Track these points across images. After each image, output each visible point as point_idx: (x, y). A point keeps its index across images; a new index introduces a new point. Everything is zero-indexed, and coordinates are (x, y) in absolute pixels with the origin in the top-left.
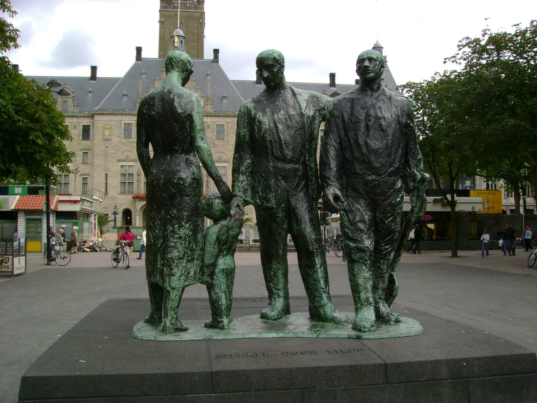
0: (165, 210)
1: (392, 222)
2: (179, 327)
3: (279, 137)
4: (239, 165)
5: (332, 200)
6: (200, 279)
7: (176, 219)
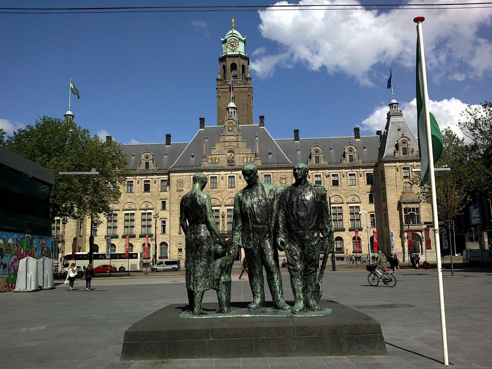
2: (201, 312)
3: (254, 211)
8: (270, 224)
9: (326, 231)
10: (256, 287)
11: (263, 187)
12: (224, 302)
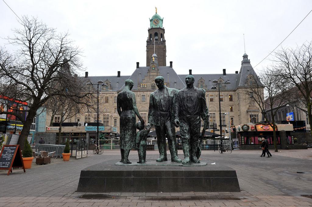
3: (161, 104)
5: (176, 124)
9: (205, 116)
11: (167, 90)
12: (142, 156)
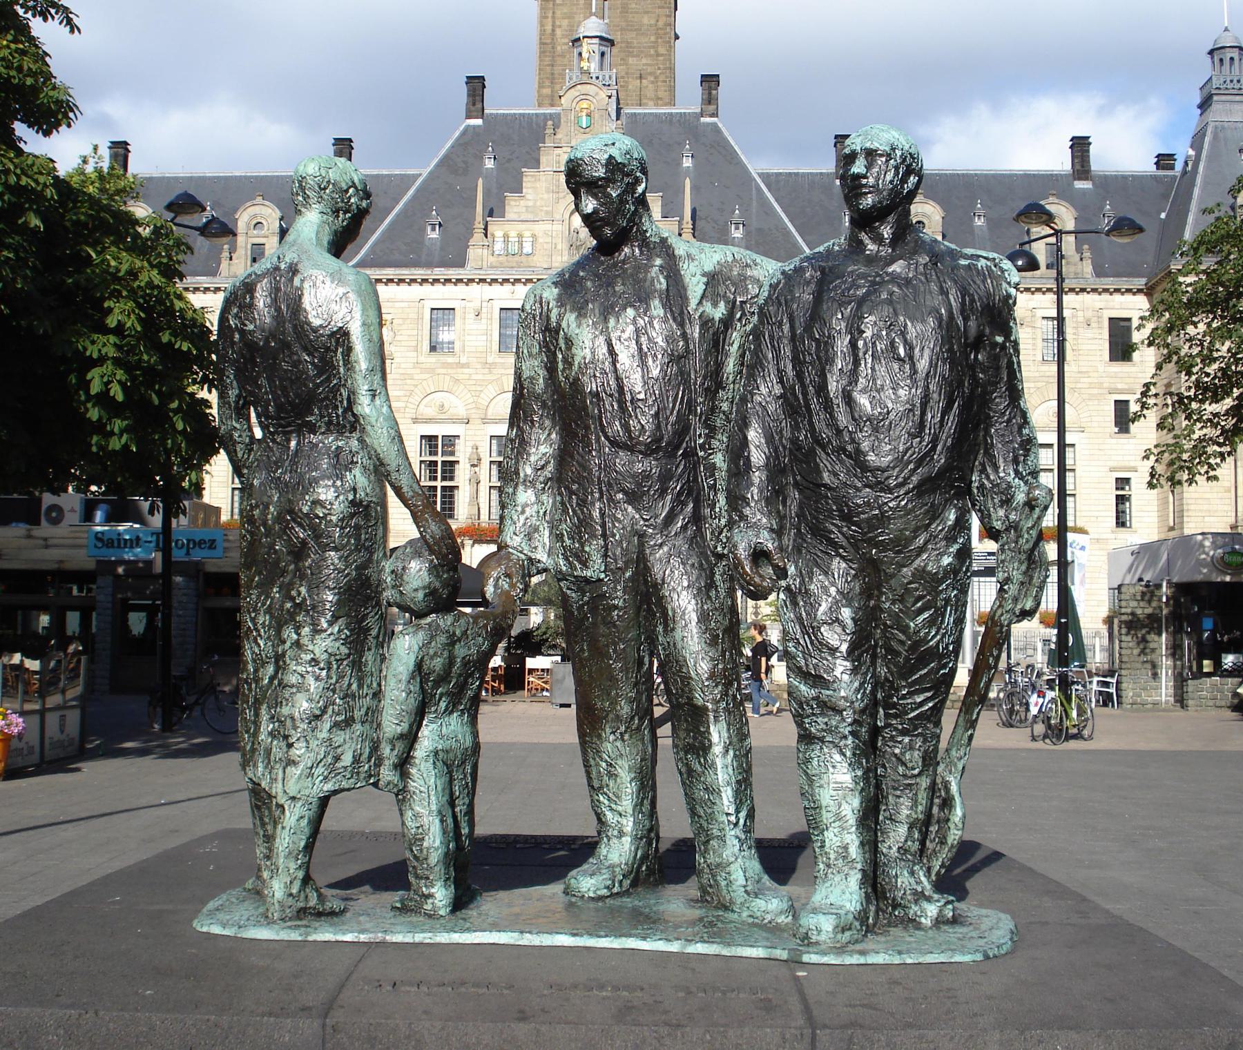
0: (280, 587)
1: (930, 627)
4: (517, 462)
6: (370, 776)
7: (308, 611)
8: (701, 454)
9: (1007, 502)
10: (611, 784)
